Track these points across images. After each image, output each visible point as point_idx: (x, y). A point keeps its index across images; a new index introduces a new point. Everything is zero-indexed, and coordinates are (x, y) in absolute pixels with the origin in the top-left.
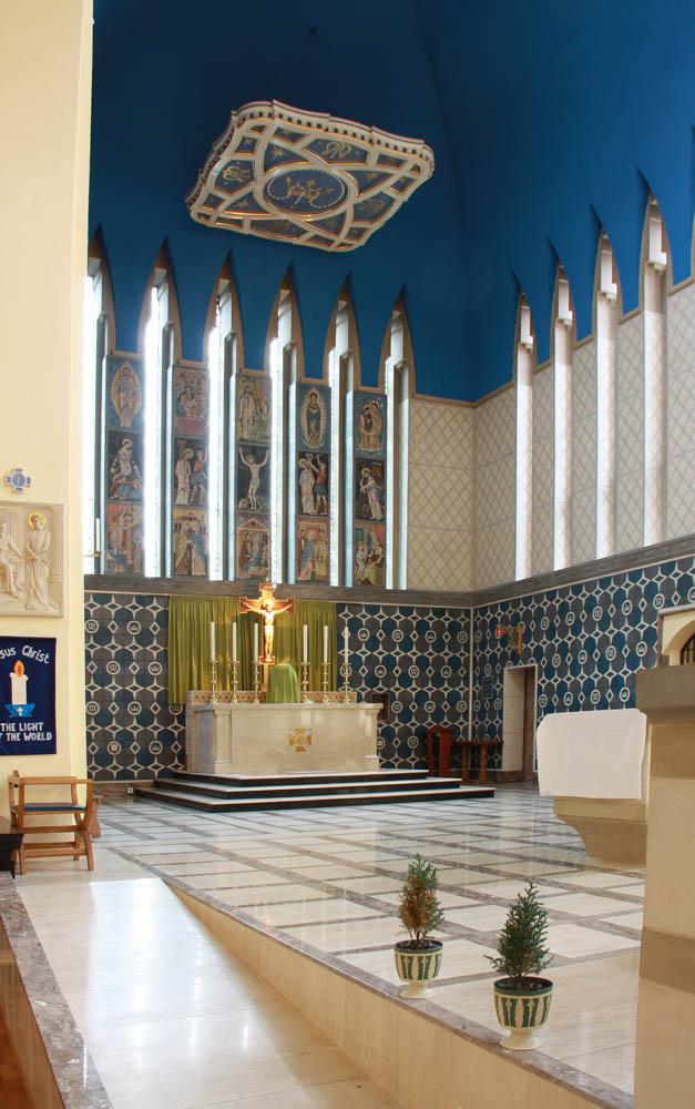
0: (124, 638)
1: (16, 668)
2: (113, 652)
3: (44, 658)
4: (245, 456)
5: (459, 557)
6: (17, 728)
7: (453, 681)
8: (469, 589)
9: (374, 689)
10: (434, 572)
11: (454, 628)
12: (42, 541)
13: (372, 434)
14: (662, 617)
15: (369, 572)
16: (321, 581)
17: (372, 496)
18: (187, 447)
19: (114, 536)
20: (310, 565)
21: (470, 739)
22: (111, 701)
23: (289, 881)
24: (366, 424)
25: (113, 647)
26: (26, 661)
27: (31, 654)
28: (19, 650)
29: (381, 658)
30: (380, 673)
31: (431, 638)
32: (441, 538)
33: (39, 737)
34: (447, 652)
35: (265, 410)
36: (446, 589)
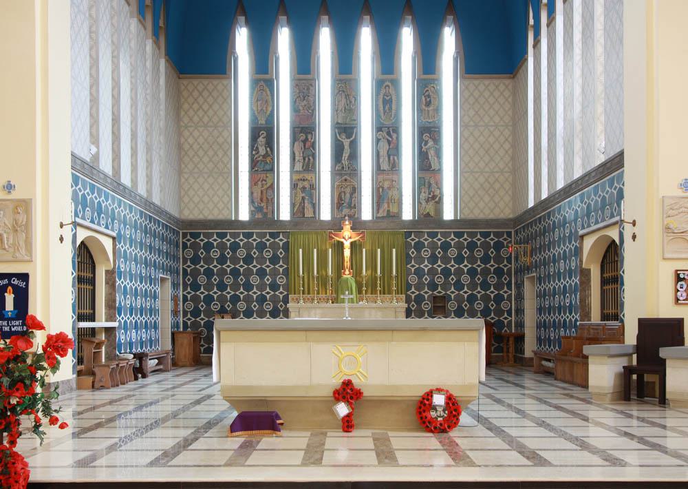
0: (261, 260)
1: (8, 291)
2: (255, 270)
3: (23, 284)
4: (339, 135)
5: (502, 193)
6: (8, 323)
7: (498, 286)
8: (511, 216)
9: (435, 292)
10: (481, 205)
11: (498, 246)
12: (21, 219)
13: (431, 108)
14: (582, 237)
15: (430, 208)
16: (394, 216)
17: (431, 153)
18: (301, 132)
19: (255, 194)
20: (386, 205)
21: (513, 331)
22: (280, 302)
23: (518, 439)
24: (426, 103)
25: (255, 266)
26: (13, 286)
27: (16, 282)
28: (9, 281)
29: (439, 269)
30: (439, 280)
31: (479, 254)
32: (487, 180)
33: (19, 329)
34: (492, 267)
35: (353, 102)
36: (491, 216)
